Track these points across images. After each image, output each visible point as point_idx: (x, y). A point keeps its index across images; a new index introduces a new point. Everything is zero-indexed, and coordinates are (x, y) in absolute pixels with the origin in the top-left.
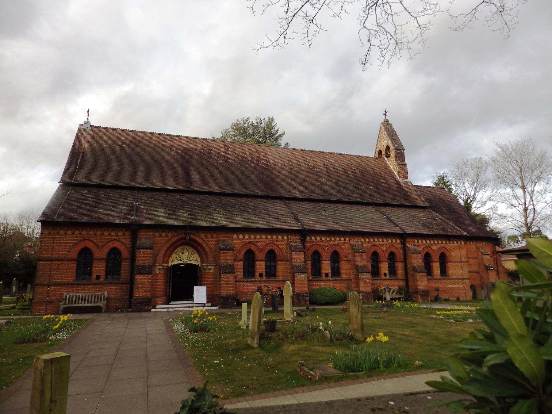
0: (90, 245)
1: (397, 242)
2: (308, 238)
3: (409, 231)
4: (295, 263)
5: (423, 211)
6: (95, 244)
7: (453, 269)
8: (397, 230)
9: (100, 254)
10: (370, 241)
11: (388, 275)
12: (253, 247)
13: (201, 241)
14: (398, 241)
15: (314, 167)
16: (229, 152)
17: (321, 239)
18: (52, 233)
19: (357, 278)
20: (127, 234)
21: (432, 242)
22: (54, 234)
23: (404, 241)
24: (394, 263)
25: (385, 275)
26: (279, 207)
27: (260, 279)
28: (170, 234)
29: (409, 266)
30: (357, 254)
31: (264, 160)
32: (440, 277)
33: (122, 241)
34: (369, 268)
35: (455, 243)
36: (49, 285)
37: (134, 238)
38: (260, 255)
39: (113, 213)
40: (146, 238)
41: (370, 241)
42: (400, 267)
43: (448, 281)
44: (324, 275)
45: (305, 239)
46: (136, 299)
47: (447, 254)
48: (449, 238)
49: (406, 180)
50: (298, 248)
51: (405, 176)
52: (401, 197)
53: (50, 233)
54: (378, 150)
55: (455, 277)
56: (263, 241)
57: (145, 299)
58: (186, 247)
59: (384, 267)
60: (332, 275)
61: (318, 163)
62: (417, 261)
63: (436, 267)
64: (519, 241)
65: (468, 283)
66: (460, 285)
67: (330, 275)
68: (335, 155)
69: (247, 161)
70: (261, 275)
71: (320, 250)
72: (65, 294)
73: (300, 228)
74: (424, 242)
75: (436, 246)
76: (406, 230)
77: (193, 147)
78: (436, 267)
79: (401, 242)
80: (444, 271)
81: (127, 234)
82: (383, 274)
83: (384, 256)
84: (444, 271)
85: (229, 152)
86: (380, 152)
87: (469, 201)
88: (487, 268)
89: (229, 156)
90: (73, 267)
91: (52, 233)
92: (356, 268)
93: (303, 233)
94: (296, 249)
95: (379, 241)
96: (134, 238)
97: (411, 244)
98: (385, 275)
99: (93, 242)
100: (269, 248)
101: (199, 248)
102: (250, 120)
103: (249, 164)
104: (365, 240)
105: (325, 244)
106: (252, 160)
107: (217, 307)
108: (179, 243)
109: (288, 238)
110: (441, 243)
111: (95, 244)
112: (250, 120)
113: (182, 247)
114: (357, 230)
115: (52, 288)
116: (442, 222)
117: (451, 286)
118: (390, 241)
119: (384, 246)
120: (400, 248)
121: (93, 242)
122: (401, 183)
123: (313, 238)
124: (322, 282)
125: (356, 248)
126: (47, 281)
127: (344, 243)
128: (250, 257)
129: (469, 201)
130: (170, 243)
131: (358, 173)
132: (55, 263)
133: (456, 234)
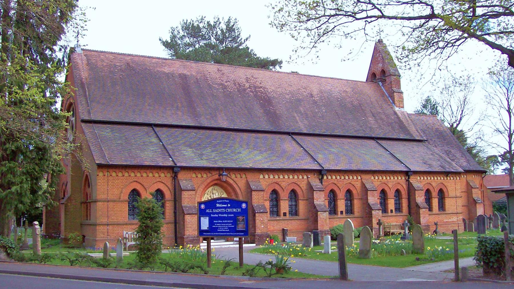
0: (138, 187)
2: (325, 177)
3: (413, 168)
6: (143, 185)
10: (378, 179)
11: (394, 211)
12: (277, 188)
13: (231, 182)
14: (403, 178)
15: (312, 96)
16: (225, 79)
17: (336, 178)
18: (106, 175)
20: (169, 175)
22: (107, 176)
23: (409, 178)
25: (392, 211)
26: (288, 144)
27: (284, 218)
29: (412, 203)
31: (261, 87)
32: (438, 212)
35: (452, 178)
37: (175, 177)
38: (284, 195)
39: (150, 155)
40: (186, 180)
41: (378, 179)
43: (444, 216)
44: (339, 213)
45: (322, 178)
46: (188, 237)
47: (445, 190)
48: (447, 174)
49: (402, 110)
50: (319, 188)
51: (401, 105)
52: (401, 134)
53: (104, 176)
55: (450, 212)
56: (286, 181)
57: (194, 237)
58: (216, 187)
61: (315, 89)
62: (420, 199)
63: (435, 202)
64: (498, 162)
65: (461, 217)
66: (454, 219)
67: (344, 213)
68: (330, 80)
69: (245, 90)
70: (285, 214)
72: (125, 233)
75: (436, 182)
77: (188, 73)
78: (435, 202)
79: (405, 179)
80: (442, 206)
81: (169, 175)
82: (390, 211)
83: (391, 194)
85: (225, 79)
87: (455, 125)
89: (226, 84)
90: (125, 207)
91: (106, 175)
93: (320, 173)
94: (317, 188)
95: (386, 179)
96: (175, 177)
97: (416, 182)
98: (392, 211)
99: (141, 184)
102: (207, 20)
103: (248, 93)
104: (375, 178)
105: (342, 183)
106: (249, 88)
107: (255, 245)
108: (212, 184)
109: (308, 178)
110: (440, 179)
111: (143, 185)
112: (207, 20)
113: (212, 187)
114: (369, 169)
115: (110, 227)
117: (447, 220)
118: (396, 178)
120: (405, 186)
121: (141, 184)
122: (398, 112)
124: (337, 219)
125: (368, 186)
127: (355, 181)
129: (455, 125)
131: (356, 103)
132: (111, 204)
133: (453, 170)
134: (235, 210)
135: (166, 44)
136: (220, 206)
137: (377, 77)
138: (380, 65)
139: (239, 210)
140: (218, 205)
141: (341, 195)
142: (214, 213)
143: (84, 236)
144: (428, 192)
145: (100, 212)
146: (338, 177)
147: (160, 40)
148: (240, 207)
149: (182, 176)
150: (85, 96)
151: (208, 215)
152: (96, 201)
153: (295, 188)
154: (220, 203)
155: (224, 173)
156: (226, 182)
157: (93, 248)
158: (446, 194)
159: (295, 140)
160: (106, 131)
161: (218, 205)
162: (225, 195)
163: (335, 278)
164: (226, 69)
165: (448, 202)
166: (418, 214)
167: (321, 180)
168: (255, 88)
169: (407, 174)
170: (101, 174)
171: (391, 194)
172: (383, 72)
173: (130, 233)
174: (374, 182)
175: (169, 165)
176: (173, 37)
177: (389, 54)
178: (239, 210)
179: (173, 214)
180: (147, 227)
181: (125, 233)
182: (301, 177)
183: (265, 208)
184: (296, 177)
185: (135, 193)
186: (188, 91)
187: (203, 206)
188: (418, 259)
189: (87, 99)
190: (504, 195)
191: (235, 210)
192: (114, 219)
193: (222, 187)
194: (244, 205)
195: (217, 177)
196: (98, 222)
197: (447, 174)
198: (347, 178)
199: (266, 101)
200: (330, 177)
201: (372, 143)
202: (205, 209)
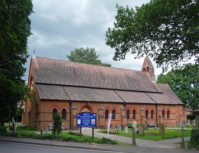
0: (56, 108)
1: (154, 107)
2: (126, 105)
4: (122, 115)
5: (161, 94)
7: (171, 116)
8: (154, 102)
9: (60, 111)
19: (142, 120)
20: (68, 103)
21: (149, 106)
23: (157, 106)
24: (129, 114)
28: (81, 104)
29: (158, 115)
30: (142, 111)
33: (67, 107)
34: (126, 117)
36: (45, 121)
37: (70, 104)
42: (155, 116)
54: (143, 68)
56: (111, 107)
59: (150, 116)
60: (133, 118)
62: (160, 114)
63: (166, 115)
66: (173, 121)
71: (129, 109)
72: (50, 124)
73: (69, 99)
74: (113, 105)
75: (166, 109)
76: (125, 101)
78: (166, 115)
80: (168, 117)
81: (68, 103)
83: (150, 112)
84: (168, 117)
86: (144, 69)
88: (181, 115)
92: (142, 116)
93: (124, 104)
96: (70, 104)
97: (159, 108)
98: (131, 118)
100: (113, 109)
101: (90, 109)
105: (131, 108)
110: (168, 107)
116: (74, 95)
119: (150, 108)
122: (153, 83)
123: (127, 105)
126: (44, 120)
128: (107, 112)
130: (82, 107)
134: (91, 117)
135: (69, 57)
136: (85, 115)
137: (146, 70)
138: (147, 65)
139: (92, 117)
140: (84, 115)
141: (131, 112)
142: (83, 118)
143: (36, 126)
144: (163, 111)
145: (42, 117)
146: (131, 105)
147: (67, 56)
148: (93, 116)
149: (73, 104)
150: (37, 74)
151: (80, 118)
152: (40, 113)
153: (115, 109)
154: (85, 114)
155: (89, 103)
156: (89, 106)
157: (38, 130)
158: (170, 112)
159: (115, 92)
160: (44, 87)
161: (84, 115)
162: (89, 111)
163: (130, 145)
164: (90, 66)
165: (171, 116)
166: (159, 119)
167: (124, 106)
168: (101, 73)
169: (156, 105)
170: (42, 103)
171: (150, 112)
172: (148, 68)
173: (51, 125)
174: (143, 108)
175: (68, 100)
176: (72, 55)
177: (108, 124)
178: (92, 117)
179: (69, 118)
180: (57, 122)
181: (50, 124)
182: (117, 105)
183: (104, 116)
184: (115, 105)
185: (55, 111)
186: (75, 73)
187: (78, 115)
188: (163, 137)
189: (37, 75)
190: (78, 120)
191: (91, 117)
192: (47, 119)
193: (88, 108)
194: (94, 115)
195: (86, 104)
196: (41, 120)
197: (170, 105)
198: (134, 106)
199: (103, 77)
200: (127, 105)
201: (143, 94)
202: (79, 117)
